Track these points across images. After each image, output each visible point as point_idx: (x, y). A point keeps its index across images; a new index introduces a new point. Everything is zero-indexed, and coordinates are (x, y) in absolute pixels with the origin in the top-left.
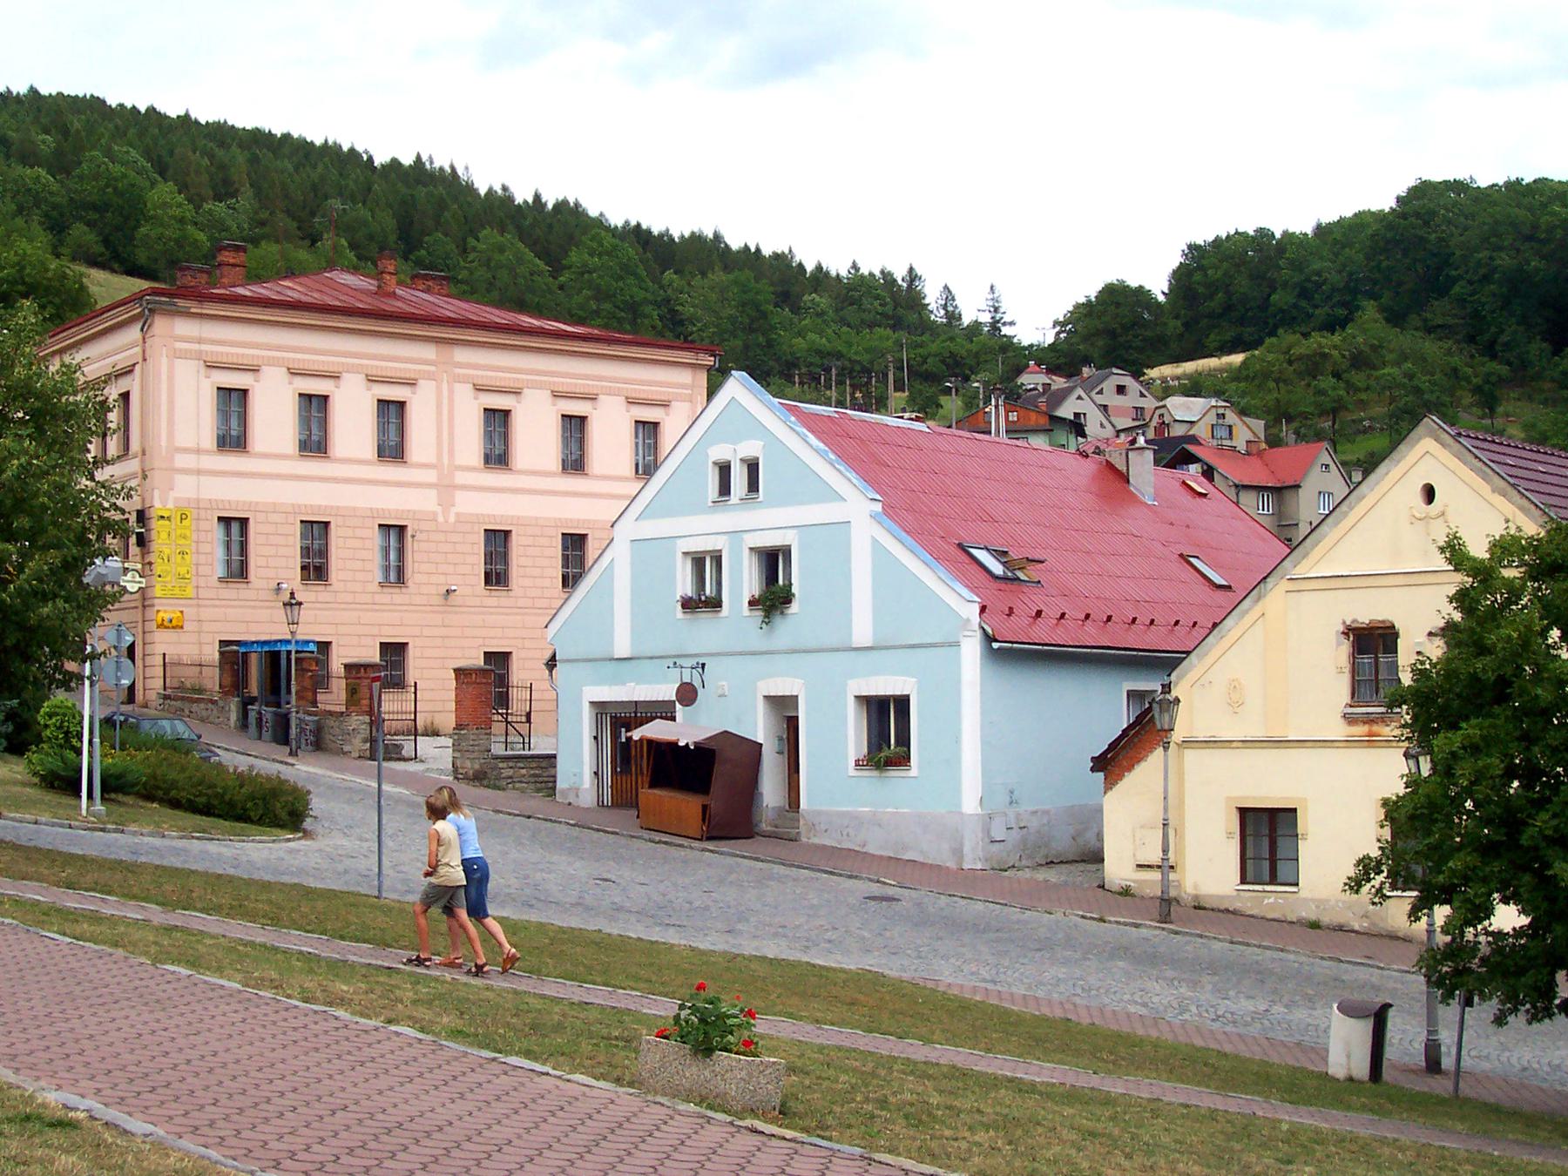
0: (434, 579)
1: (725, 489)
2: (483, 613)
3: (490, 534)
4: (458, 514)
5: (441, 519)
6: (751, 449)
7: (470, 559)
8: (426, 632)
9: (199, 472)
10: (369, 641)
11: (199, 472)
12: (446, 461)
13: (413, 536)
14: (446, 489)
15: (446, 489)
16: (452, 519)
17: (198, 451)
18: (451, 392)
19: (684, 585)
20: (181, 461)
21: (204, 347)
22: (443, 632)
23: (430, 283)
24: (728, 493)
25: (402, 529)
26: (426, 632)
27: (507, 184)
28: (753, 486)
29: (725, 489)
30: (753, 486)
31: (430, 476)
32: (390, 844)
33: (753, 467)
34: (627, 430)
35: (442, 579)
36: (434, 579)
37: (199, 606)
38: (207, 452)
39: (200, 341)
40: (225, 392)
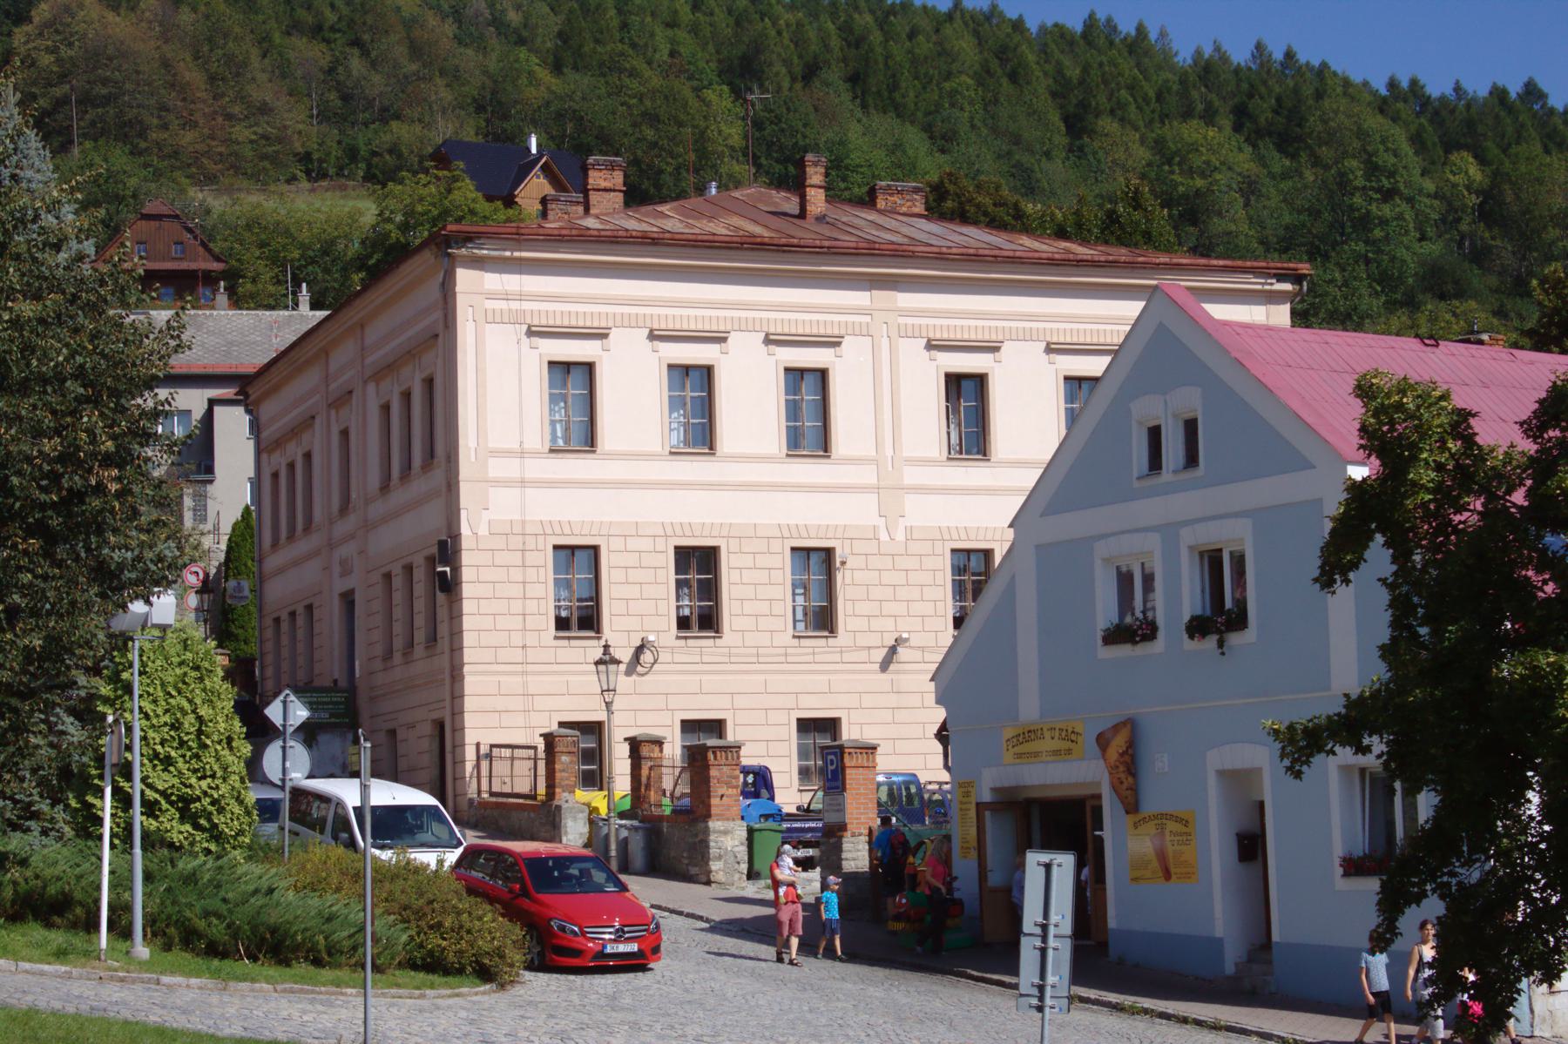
0: (877, 624)
1: (1155, 463)
2: (498, 673)
3: (802, 554)
4: (909, 530)
5: (884, 536)
6: (1189, 400)
7: (930, 593)
8: (868, 701)
9: (523, 483)
10: (782, 717)
11: (523, 483)
12: (889, 452)
13: (843, 563)
14: (889, 491)
15: (889, 491)
16: (900, 536)
17: (522, 454)
18: (892, 350)
19: (1106, 612)
20: (497, 469)
21: (527, 306)
22: (893, 700)
23: (895, 198)
24: (1160, 468)
25: (828, 553)
26: (868, 701)
27: (1295, 48)
28: (1192, 459)
29: (1155, 463)
30: (1192, 459)
31: (868, 476)
32: (373, 1010)
33: (1191, 427)
34: (536, 382)
35: (889, 624)
36: (877, 624)
37: (524, 673)
38: (535, 454)
39: (521, 297)
40: (795, 375)
